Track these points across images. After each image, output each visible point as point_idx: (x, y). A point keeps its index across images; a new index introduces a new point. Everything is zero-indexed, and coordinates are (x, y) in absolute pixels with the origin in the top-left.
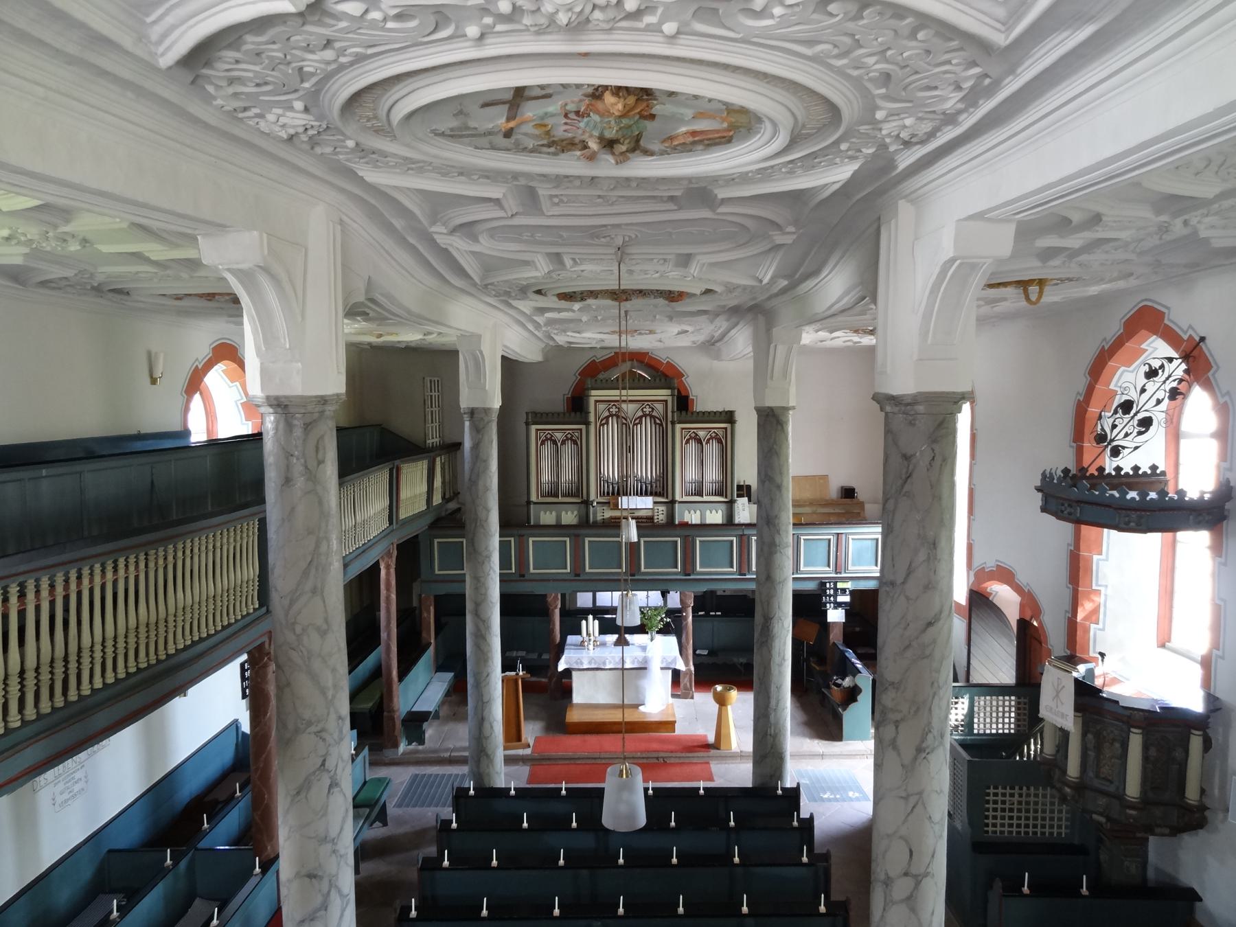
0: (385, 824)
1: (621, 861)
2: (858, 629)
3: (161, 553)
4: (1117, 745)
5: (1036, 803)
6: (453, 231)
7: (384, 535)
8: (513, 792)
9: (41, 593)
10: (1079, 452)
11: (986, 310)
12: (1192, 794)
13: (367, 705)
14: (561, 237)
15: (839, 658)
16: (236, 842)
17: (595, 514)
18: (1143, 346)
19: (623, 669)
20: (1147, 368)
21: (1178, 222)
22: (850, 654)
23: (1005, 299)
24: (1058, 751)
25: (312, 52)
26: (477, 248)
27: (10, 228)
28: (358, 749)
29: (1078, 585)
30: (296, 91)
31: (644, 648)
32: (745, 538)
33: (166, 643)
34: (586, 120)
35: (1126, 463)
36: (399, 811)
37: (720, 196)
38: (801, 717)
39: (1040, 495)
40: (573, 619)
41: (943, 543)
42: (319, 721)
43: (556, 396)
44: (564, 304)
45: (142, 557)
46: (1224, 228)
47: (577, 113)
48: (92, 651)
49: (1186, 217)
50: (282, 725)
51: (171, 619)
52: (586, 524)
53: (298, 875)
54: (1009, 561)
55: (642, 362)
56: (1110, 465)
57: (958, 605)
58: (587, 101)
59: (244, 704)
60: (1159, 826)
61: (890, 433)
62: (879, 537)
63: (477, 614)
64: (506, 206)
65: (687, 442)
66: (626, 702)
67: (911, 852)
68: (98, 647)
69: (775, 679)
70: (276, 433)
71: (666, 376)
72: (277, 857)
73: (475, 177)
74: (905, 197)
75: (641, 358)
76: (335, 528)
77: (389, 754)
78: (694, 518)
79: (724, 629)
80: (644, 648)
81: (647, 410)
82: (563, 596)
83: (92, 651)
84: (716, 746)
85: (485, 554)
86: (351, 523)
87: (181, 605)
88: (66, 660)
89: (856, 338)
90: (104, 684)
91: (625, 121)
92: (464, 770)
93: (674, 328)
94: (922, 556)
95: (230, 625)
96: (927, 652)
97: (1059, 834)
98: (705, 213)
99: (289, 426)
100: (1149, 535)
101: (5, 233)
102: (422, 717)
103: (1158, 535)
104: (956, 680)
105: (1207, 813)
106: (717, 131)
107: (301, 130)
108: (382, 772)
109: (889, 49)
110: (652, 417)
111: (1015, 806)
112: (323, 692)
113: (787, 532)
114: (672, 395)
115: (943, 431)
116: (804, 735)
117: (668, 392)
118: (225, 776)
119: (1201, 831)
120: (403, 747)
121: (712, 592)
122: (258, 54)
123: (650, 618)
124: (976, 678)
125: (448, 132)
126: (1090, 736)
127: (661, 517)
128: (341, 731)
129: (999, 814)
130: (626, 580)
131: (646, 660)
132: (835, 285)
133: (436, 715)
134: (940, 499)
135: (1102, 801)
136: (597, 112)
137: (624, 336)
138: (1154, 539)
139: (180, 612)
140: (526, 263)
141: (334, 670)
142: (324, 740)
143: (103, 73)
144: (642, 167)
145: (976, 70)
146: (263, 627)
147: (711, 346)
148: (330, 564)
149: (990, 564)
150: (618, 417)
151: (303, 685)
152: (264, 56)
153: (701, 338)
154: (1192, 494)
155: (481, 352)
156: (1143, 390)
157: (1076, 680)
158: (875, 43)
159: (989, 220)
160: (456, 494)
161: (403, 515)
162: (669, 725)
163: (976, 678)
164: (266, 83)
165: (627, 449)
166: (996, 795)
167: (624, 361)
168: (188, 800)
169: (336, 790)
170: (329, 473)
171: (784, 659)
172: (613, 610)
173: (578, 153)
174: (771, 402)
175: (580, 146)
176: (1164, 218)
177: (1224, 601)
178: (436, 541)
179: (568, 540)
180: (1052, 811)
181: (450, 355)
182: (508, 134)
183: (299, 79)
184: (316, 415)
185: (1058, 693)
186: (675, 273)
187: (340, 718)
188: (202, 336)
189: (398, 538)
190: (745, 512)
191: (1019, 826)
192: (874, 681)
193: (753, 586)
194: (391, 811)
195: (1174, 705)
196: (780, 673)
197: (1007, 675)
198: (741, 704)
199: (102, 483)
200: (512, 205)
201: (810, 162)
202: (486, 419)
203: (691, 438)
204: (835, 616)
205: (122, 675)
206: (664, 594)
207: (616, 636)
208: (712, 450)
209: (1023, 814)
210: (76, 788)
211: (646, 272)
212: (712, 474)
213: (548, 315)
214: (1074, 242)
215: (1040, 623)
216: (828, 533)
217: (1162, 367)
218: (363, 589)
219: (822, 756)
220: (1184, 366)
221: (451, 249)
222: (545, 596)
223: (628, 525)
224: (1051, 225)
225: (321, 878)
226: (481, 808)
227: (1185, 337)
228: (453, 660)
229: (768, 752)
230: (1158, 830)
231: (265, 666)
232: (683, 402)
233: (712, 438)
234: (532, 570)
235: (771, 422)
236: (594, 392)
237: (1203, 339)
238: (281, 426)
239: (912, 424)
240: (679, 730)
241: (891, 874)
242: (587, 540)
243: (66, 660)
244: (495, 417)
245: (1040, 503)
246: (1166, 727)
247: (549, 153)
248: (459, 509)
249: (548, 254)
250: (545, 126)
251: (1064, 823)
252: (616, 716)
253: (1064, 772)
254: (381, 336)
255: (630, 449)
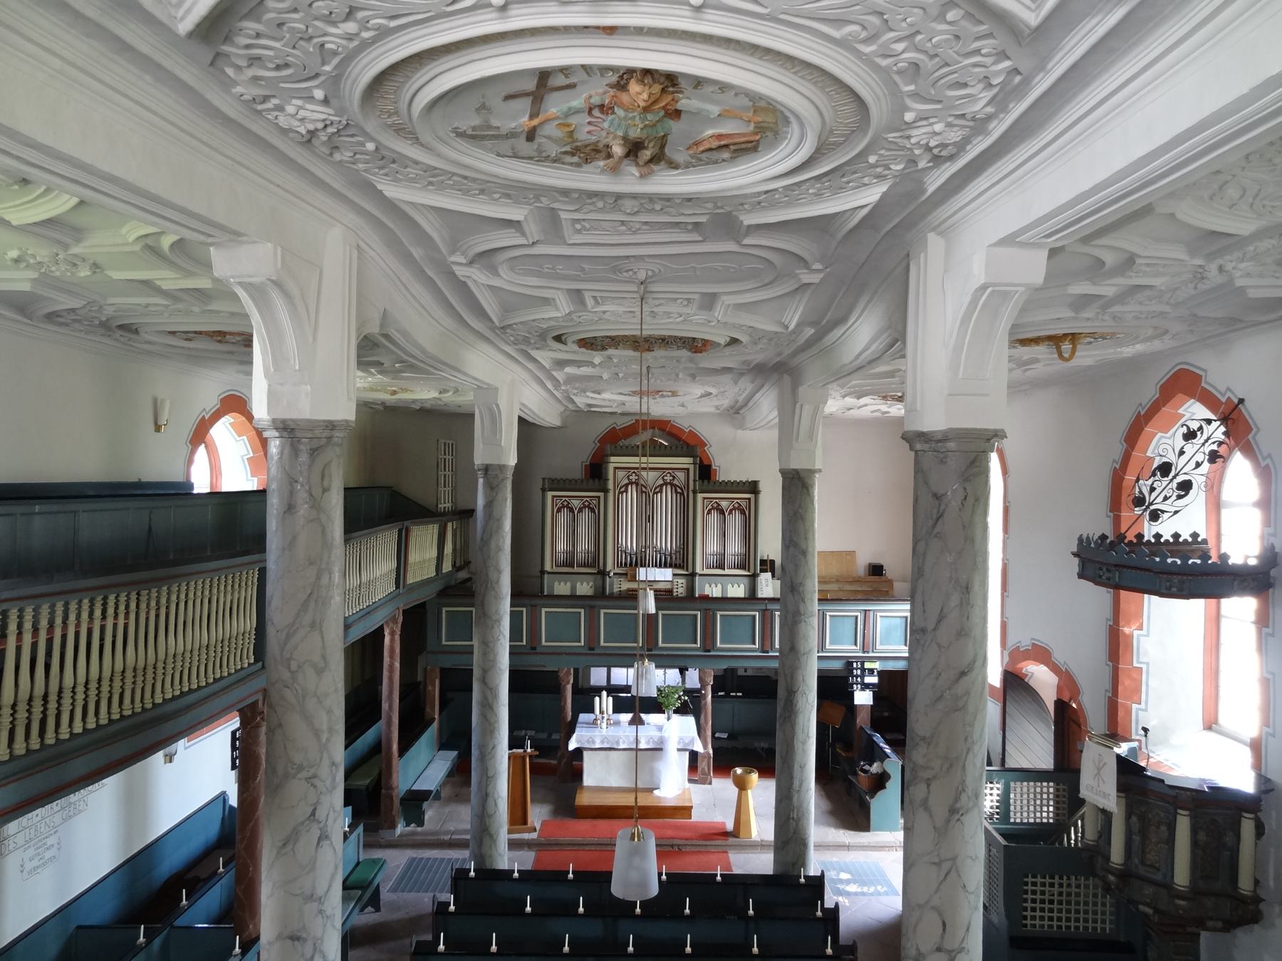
0: (378, 909)
1: (631, 949)
2: (886, 714)
3: (154, 595)
4: (1163, 828)
5: (1078, 895)
6: (471, 263)
7: (390, 598)
8: (516, 875)
9: (27, 624)
10: (1117, 521)
11: (1018, 373)
12: (1245, 884)
13: (363, 782)
14: (583, 269)
15: (868, 743)
16: (219, 920)
17: (612, 585)
18: (1180, 411)
19: (637, 750)
20: (1185, 430)
21: (1213, 268)
22: (878, 738)
23: (1036, 361)
24: (1100, 837)
25: (334, 24)
26: (496, 282)
27: (20, 249)
28: (353, 826)
29: (1118, 662)
30: (317, 76)
31: (660, 728)
32: (768, 614)
33: (153, 692)
34: (610, 117)
35: (1165, 528)
36: (393, 896)
37: (746, 223)
38: (826, 805)
39: (1076, 560)
40: (585, 698)
41: (976, 587)
42: (311, 766)
43: (574, 463)
44: (583, 354)
45: (134, 596)
46: (1261, 276)
47: (601, 107)
48: (74, 692)
49: (1220, 261)
50: (272, 769)
51: (160, 665)
52: (601, 595)
53: (280, 937)
54: (1045, 639)
55: (663, 430)
56: (1149, 531)
57: (992, 687)
58: (612, 92)
59: (233, 775)
60: (1211, 919)
61: (920, 472)
62: (908, 614)
63: (484, 681)
64: (528, 233)
65: (709, 512)
66: (640, 785)
67: (944, 925)
68: (80, 689)
69: (798, 758)
70: (281, 458)
71: (688, 445)
72: (258, 938)
73: (496, 196)
74: (933, 229)
75: (662, 426)
76: (341, 587)
77: (385, 835)
78: (715, 591)
79: (744, 711)
80: (660, 728)
81: (668, 478)
82: (576, 671)
83: (74, 692)
84: (735, 834)
85: (494, 618)
86: (356, 582)
87: (171, 652)
88: (45, 698)
89: (884, 408)
90: (84, 729)
91: (650, 117)
92: (466, 854)
93: (698, 390)
94: (955, 600)
95: (222, 678)
96: (960, 704)
97: (1103, 929)
98: (731, 246)
99: (295, 451)
100: (1192, 601)
101: (14, 254)
102: (422, 796)
103: (1202, 601)
104: (989, 764)
105: (1262, 906)
106: (744, 135)
107: (320, 125)
108: (378, 854)
109: (918, 32)
110: (672, 485)
111: (1056, 898)
112: (317, 734)
113: (812, 600)
114: (694, 463)
115: (975, 473)
116: (829, 825)
117: (690, 460)
118: (209, 853)
119: (1256, 927)
120: (400, 828)
121: (732, 671)
122: (280, 25)
123: (667, 696)
124: (1010, 763)
125: (470, 132)
126: (1134, 819)
127: (681, 590)
128: (334, 779)
129: (1038, 905)
130: (642, 656)
131: (662, 740)
132: (862, 333)
133: (438, 796)
134: (973, 541)
135: (1149, 890)
136: (622, 106)
137: (645, 399)
138: (1196, 607)
139: (170, 660)
140: (546, 301)
141: (329, 712)
142: (315, 787)
143: (125, 48)
144: (668, 183)
145: (1006, 64)
146: (259, 683)
147: (736, 413)
148: (331, 598)
149: (1026, 643)
150: (637, 485)
151: (296, 727)
152: (285, 28)
153: (725, 402)
154: (1236, 559)
155: (498, 406)
156: (1182, 453)
157: (1118, 756)
158: (904, 24)
159: (1023, 245)
160: (467, 564)
161: (411, 580)
162: (685, 811)
163: (1010, 763)
164: (287, 65)
165: (646, 518)
166: (1034, 884)
167: (644, 428)
168: (166, 877)
169: (325, 843)
170: (334, 501)
171: (808, 736)
172: (627, 689)
173: (602, 163)
174: (795, 464)
175: (603, 154)
176: (1198, 261)
177: (1273, 674)
178: (444, 610)
179: (582, 611)
180: (1095, 904)
181: (463, 419)
182: (531, 136)
183: (319, 60)
184: (323, 441)
185: (1099, 770)
186: (700, 317)
187: (333, 764)
188: (209, 386)
189: (403, 604)
190: (768, 586)
191: (1059, 919)
192: (903, 767)
193: (775, 664)
194: (385, 895)
195: (1222, 785)
196: (804, 751)
197: (1045, 760)
198: (762, 793)
199: (96, 525)
200: (533, 230)
201: (836, 179)
202: (501, 477)
203: (713, 508)
204: (863, 698)
205: (104, 721)
206: (683, 671)
207: (630, 716)
208: (735, 521)
209: (1064, 915)
210: (48, 855)
211: (668, 314)
212: (734, 547)
213: (568, 370)
214: (1107, 289)
215: (1079, 704)
216: (855, 610)
217: (1201, 428)
218: (364, 653)
219: (848, 847)
220: (1223, 429)
221: (470, 283)
222: (556, 673)
223: (646, 596)
224: (1086, 247)
225: (305, 940)
226: (481, 891)
227: (1223, 400)
228: (458, 739)
229: (789, 837)
230: (1210, 924)
231: (258, 726)
232: (706, 471)
233: (734, 509)
234: (544, 643)
235: (797, 486)
236: (613, 459)
237: (1241, 401)
238: (287, 451)
239: (942, 462)
240: (696, 816)
241: (923, 950)
242: (602, 611)
243: (45, 698)
244: (510, 474)
245: (1076, 569)
246: (1214, 809)
247: (571, 164)
248: (470, 579)
249: (568, 290)
250: (569, 126)
251: (1108, 918)
252: (628, 800)
253: (1108, 858)
254: (394, 393)
255: (650, 519)
